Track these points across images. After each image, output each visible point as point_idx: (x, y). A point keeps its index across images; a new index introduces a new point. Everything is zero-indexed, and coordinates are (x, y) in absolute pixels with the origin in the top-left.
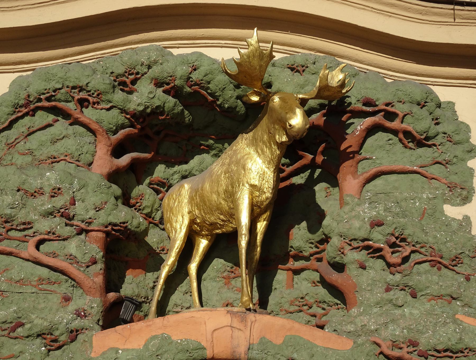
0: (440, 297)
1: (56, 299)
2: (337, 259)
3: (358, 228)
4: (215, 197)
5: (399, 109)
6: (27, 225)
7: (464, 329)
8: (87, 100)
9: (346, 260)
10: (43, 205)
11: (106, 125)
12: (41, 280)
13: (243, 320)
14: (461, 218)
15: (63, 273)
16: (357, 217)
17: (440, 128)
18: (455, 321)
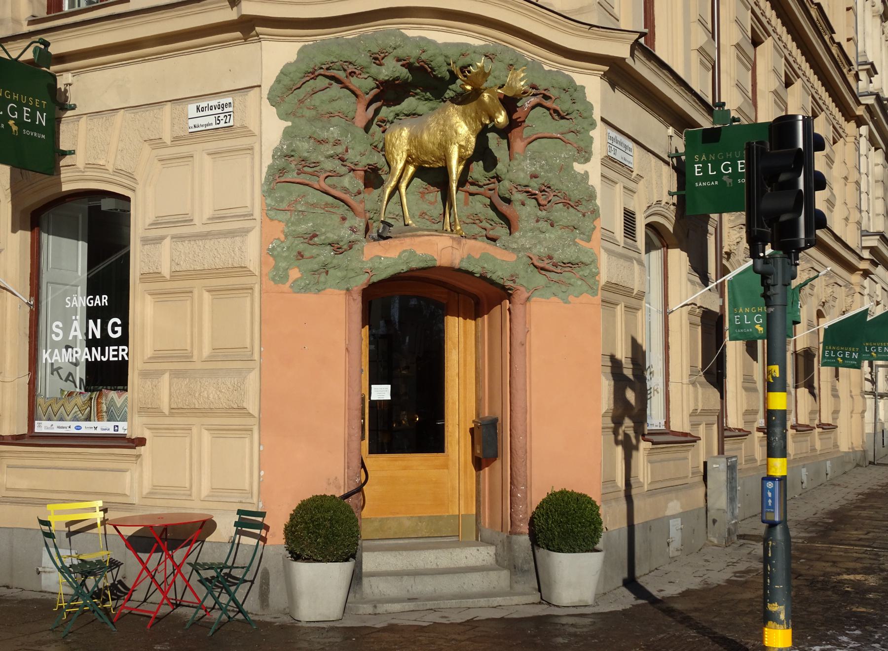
0: (567, 227)
1: (337, 219)
2: (507, 196)
3: (522, 177)
4: (431, 145)
5: (553, 93)
6: (317, 163)
7: (579, 250)
8: (355, 73)
9: (513, 198)
11: (364, 90)
13: (459, 243)
15: (342, 201)
16: (523, 170)
17: (576, 107)
18: (575, 244)
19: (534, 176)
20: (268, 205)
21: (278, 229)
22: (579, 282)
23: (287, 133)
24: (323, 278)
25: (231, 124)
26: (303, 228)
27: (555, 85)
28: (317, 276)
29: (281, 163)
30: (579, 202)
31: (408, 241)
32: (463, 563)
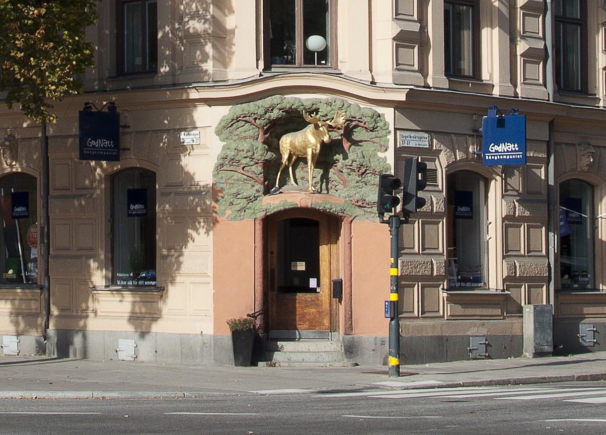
1: (250, 185)
6: (239, 161)
10: (244, 155)
12: (244, 179)
14: (383, 157)
23: (224, 148)
29: (221, 161)
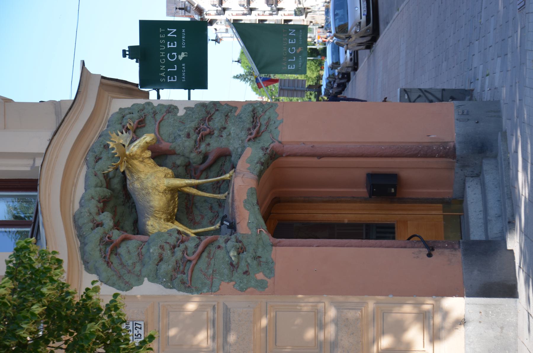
1: (218, 252)
3: (189, 143)
9: (204, 151)
19: (188, 136)
20: (208, 291)
21: (226, 286)
22: (267, 113)
24: (263, 259)
25: (142, 323)
26: (226, 271)
27: (120, 122)
28: (262, 263)
30: (208, 113)
31: (236, 204)
32: (479, 206)
